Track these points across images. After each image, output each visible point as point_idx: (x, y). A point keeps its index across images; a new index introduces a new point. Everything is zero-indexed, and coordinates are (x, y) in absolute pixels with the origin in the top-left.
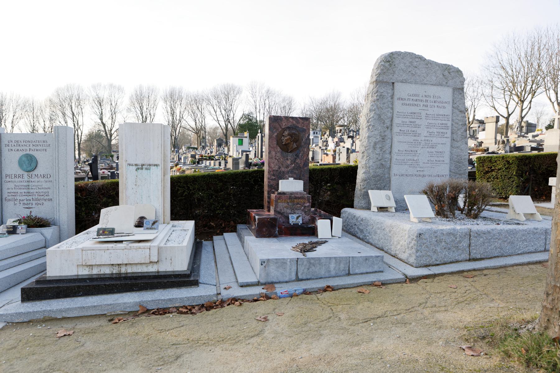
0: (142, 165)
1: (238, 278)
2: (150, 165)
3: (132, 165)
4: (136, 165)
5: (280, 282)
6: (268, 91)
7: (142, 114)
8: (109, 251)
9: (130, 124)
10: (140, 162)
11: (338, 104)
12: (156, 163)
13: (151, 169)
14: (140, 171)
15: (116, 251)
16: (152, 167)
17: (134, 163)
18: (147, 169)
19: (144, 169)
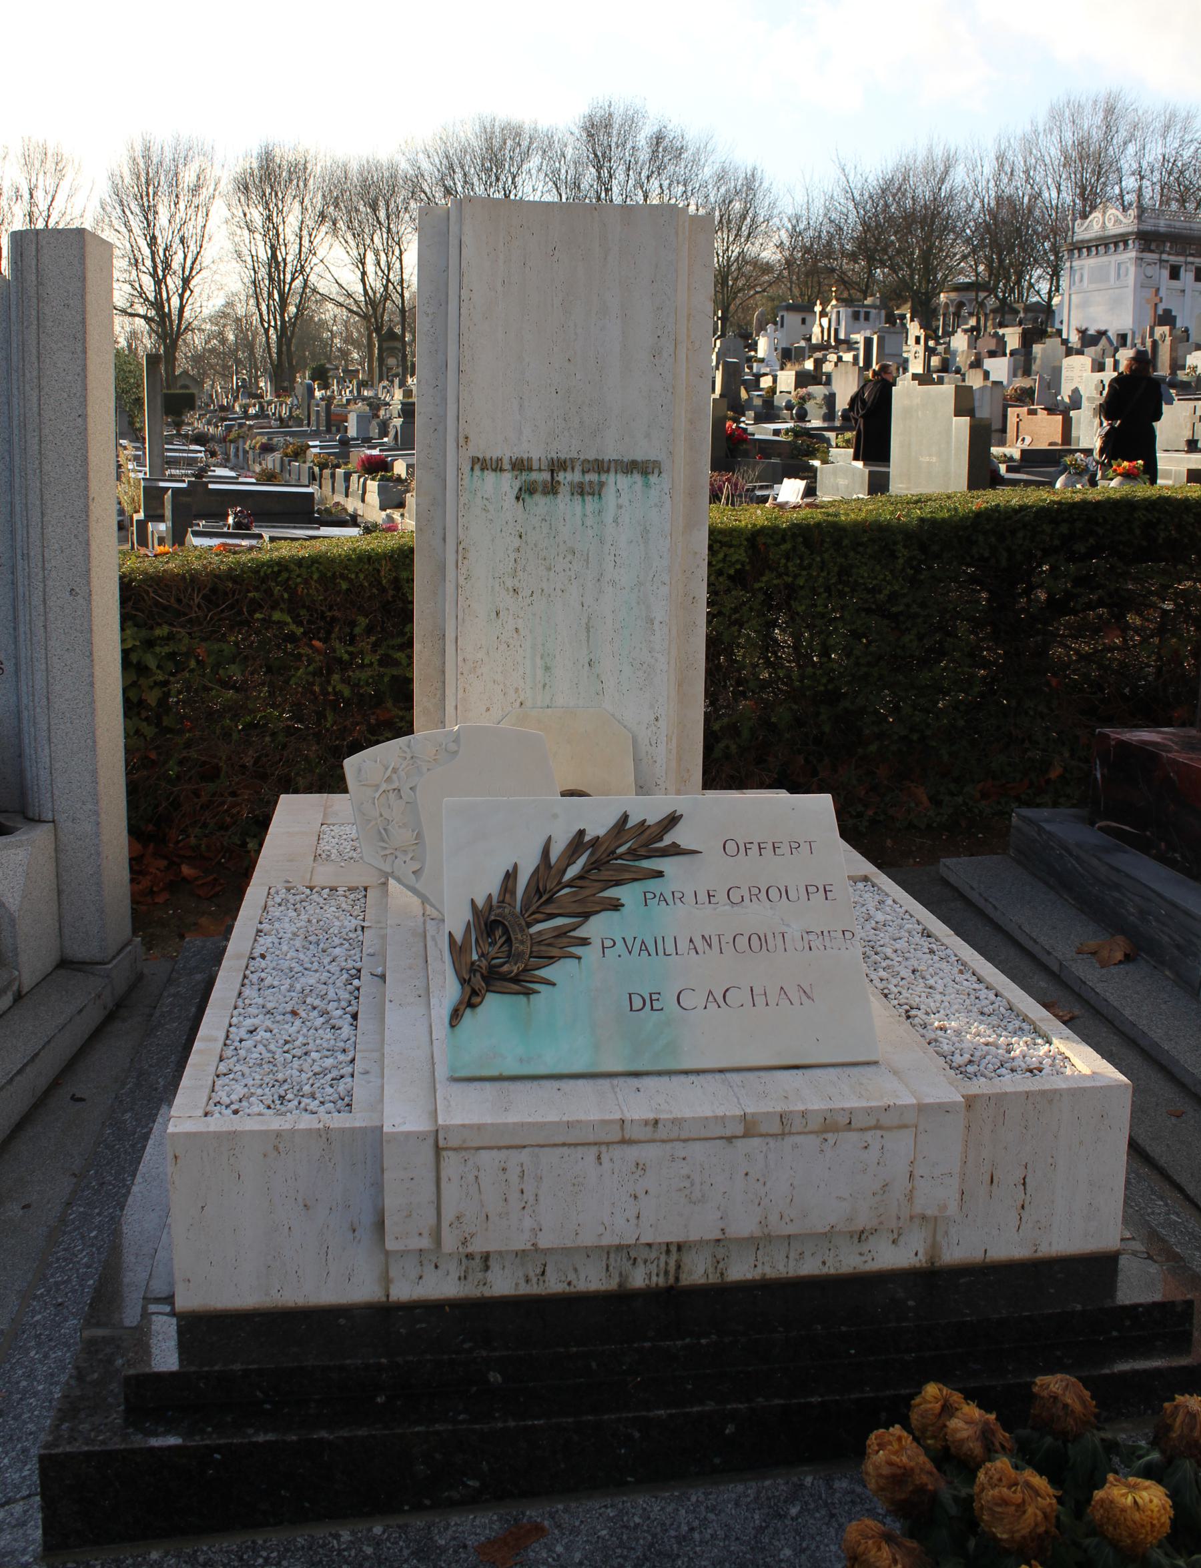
0: (557, 466)
1: (771, 1132)
2: (600, 466)
3: (497, 467)
4: (520, 466)
5: (56, 830)
6: (659, 139)
7: (153, 242)
8: (632, 1153)
9: (548, 203)
10: (535, 450)
11: (951, 197)
12: (639, 456)
13: (609, 493)
14: (540, 503)
15: (680, 1150)
16: (616, 483)
17: (505, 452)
18: (581, 490)
19: (564, 490)
